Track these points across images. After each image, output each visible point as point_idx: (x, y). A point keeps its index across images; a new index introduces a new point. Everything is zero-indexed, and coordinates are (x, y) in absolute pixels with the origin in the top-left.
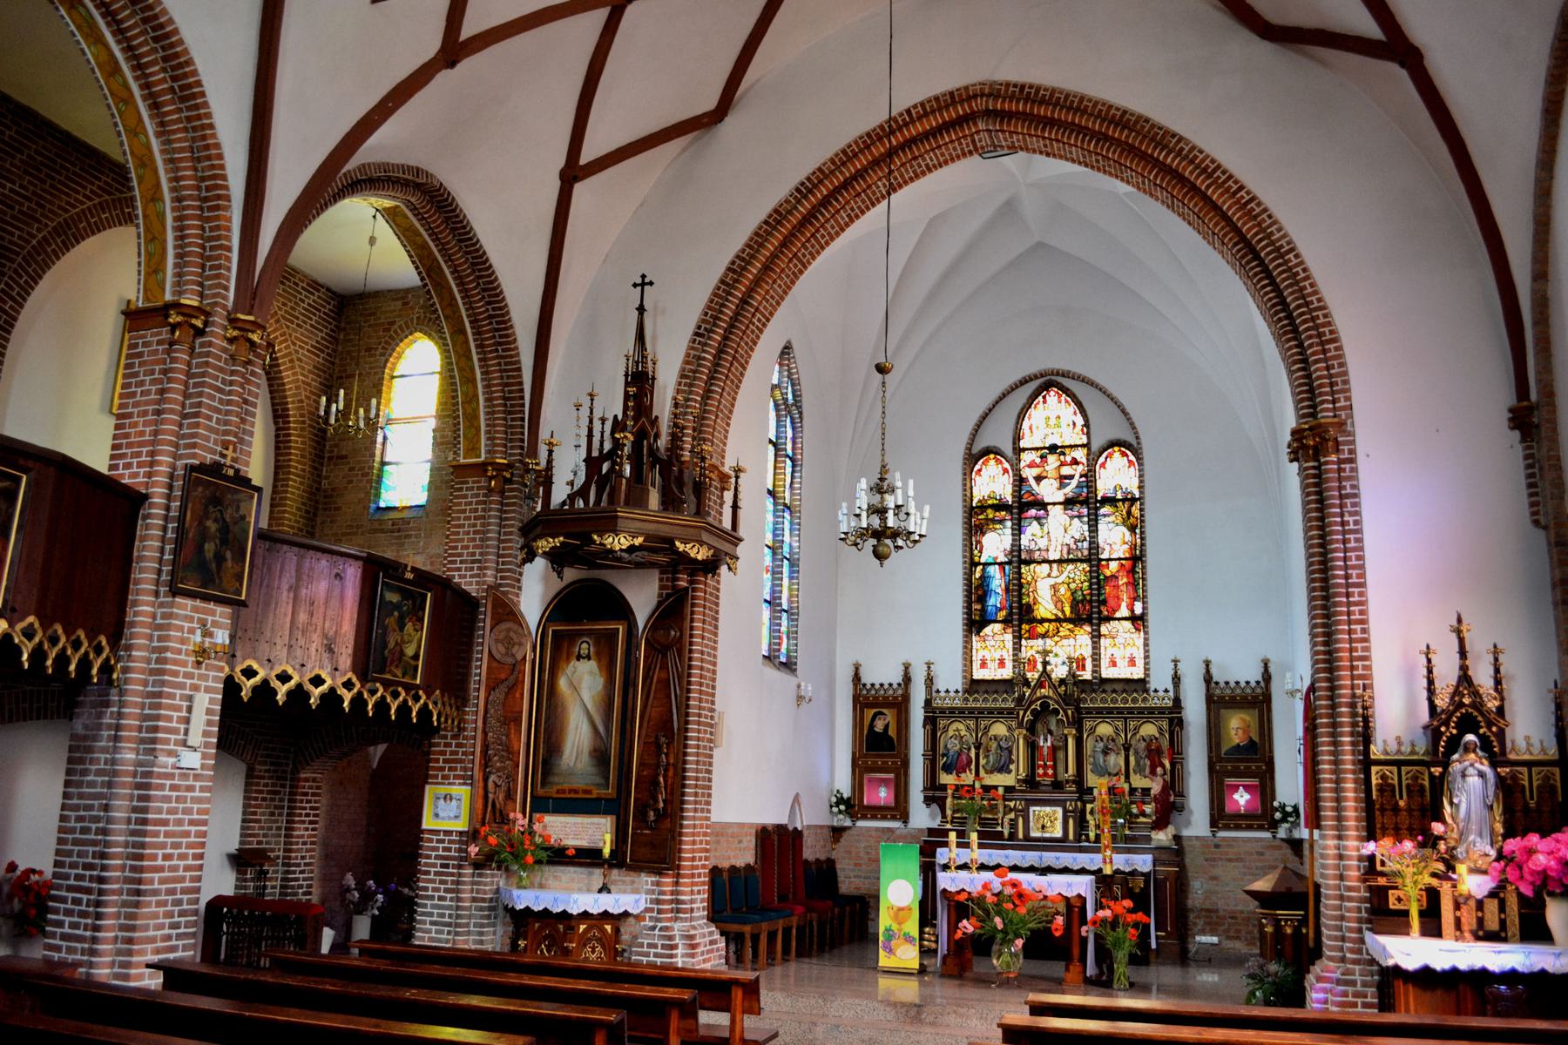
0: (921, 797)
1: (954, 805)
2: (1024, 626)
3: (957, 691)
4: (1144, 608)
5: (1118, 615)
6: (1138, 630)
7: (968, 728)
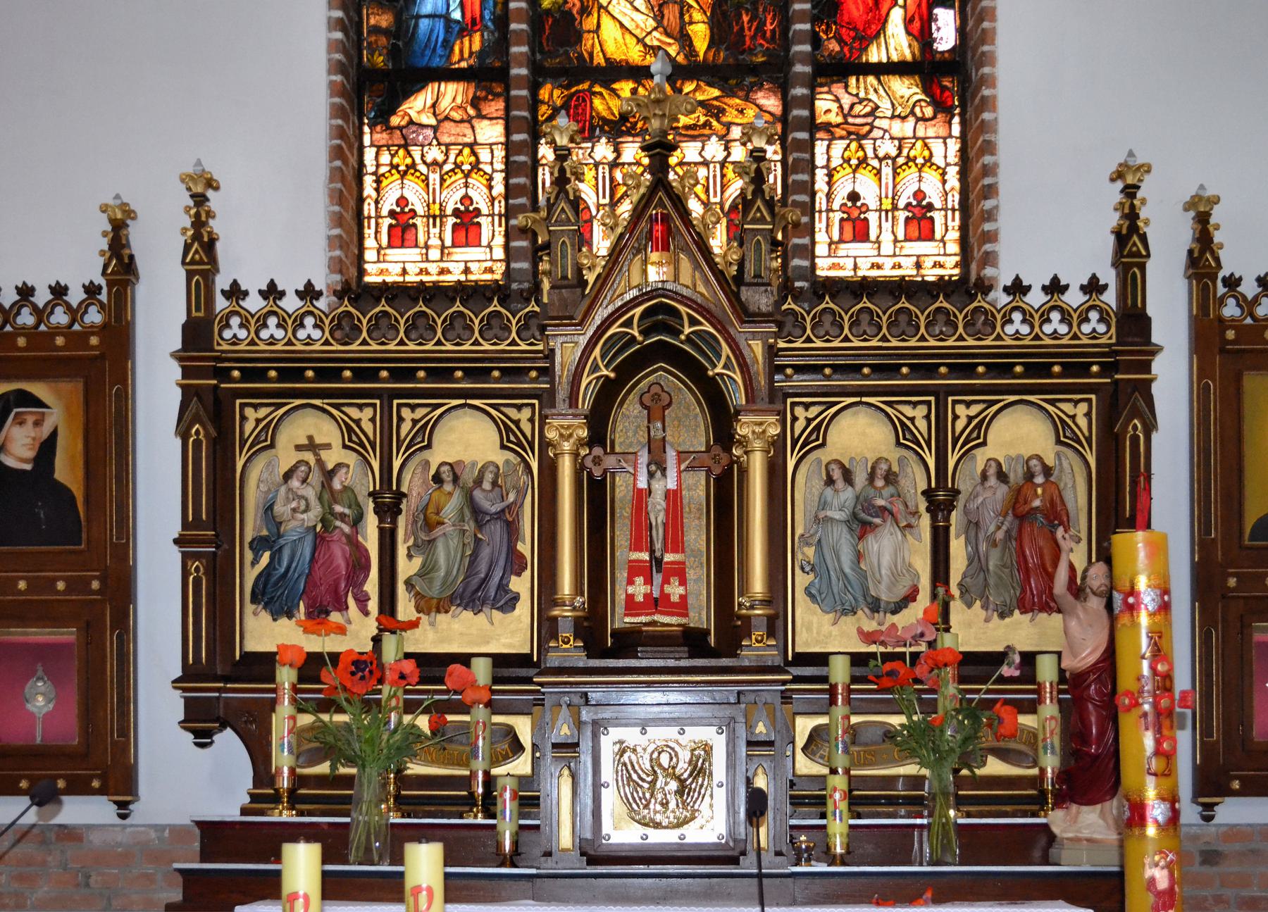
0: (175, 705)
1: (299, 734)
2: (544, 93)
3: (309, 293)
4: (962, 31)
5: (875, 55)
6: (942, 107)
7: (350, 431)
